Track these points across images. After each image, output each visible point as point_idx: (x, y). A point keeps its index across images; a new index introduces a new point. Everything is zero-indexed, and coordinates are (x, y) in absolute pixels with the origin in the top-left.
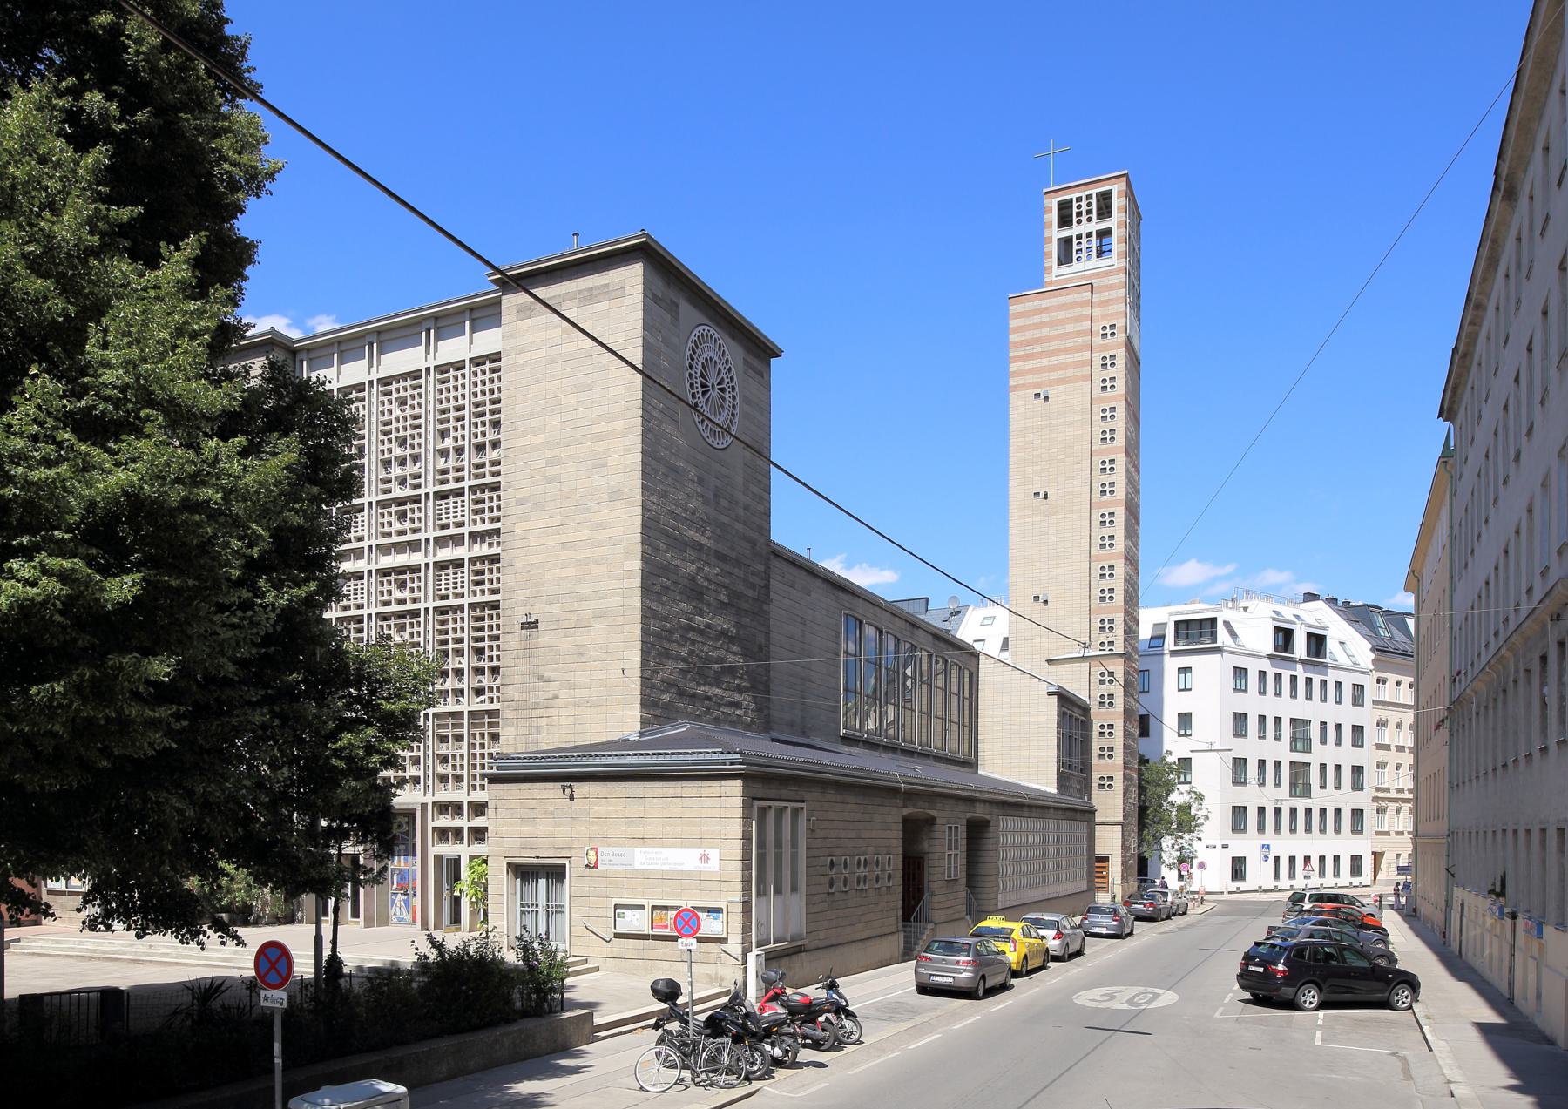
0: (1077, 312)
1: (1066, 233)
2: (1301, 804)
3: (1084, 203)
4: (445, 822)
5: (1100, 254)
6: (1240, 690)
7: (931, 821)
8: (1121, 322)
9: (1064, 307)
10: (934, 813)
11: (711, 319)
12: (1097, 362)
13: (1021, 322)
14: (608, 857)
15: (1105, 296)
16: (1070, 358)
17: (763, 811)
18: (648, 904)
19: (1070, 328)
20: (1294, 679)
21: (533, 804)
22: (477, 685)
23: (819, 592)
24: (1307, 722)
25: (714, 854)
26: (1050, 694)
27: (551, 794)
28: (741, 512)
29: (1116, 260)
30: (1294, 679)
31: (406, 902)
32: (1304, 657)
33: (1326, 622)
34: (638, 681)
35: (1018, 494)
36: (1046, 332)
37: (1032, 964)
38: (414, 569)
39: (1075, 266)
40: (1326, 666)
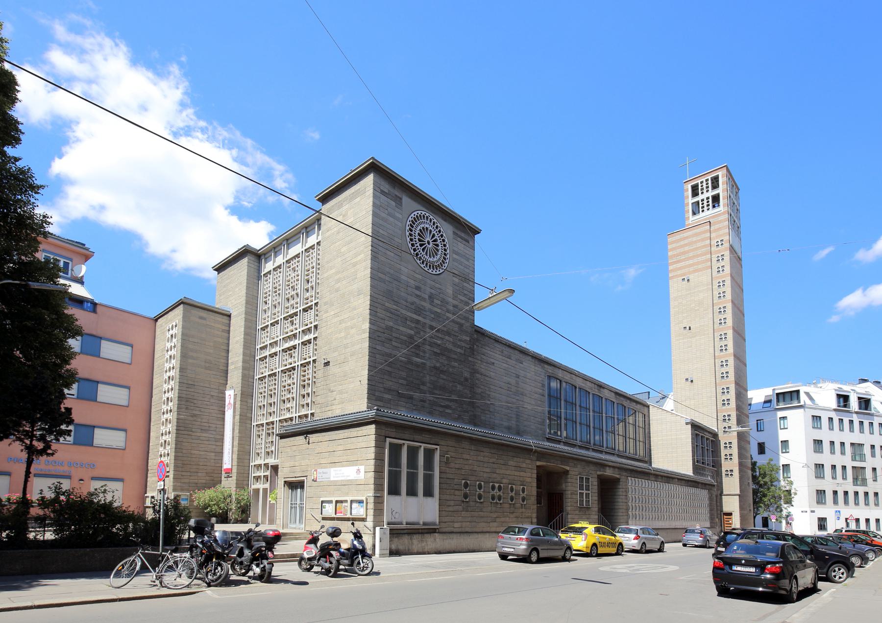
0: (703, 236)
1: (696, 199)
2: (861, 490)
3: (704, 184)
5: (714, 207)
6: (817, 428)
7: (566, 472)
8: (726, 238)
9: (696, 235)
10: (568, 468)
11: (424, 206)
12: (714, 259)
13: (674, 245)
15: (717, 226)
16: (700, 259)
17: (395, 451)
18: (334, 499)
19: (699, 244)
20: (851, 422)
22: (302, 393)
23: (528, 363)
24: (862, 445)
25: (362, 468)
26: (687, 424)
28: (451, 308)
29: (723, 207)
30: (851, 422)
32: (857, 409)
33: (872, 393)
34: (366, 386)
35: (675, 328)
36: (686, 249)
37: (601, 550)
38: (294, 347)
39: (701, 215)
40: (872, 415)
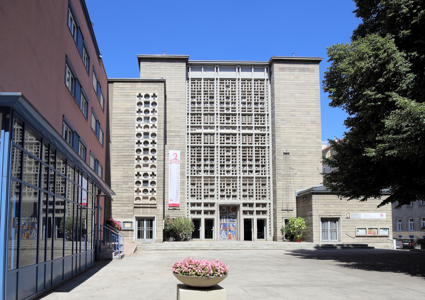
4: (247, 208)
14: (353, 215)
21: (328, 201)
25: (384, 214)
27: (334, 198)
31: (226, 233)
